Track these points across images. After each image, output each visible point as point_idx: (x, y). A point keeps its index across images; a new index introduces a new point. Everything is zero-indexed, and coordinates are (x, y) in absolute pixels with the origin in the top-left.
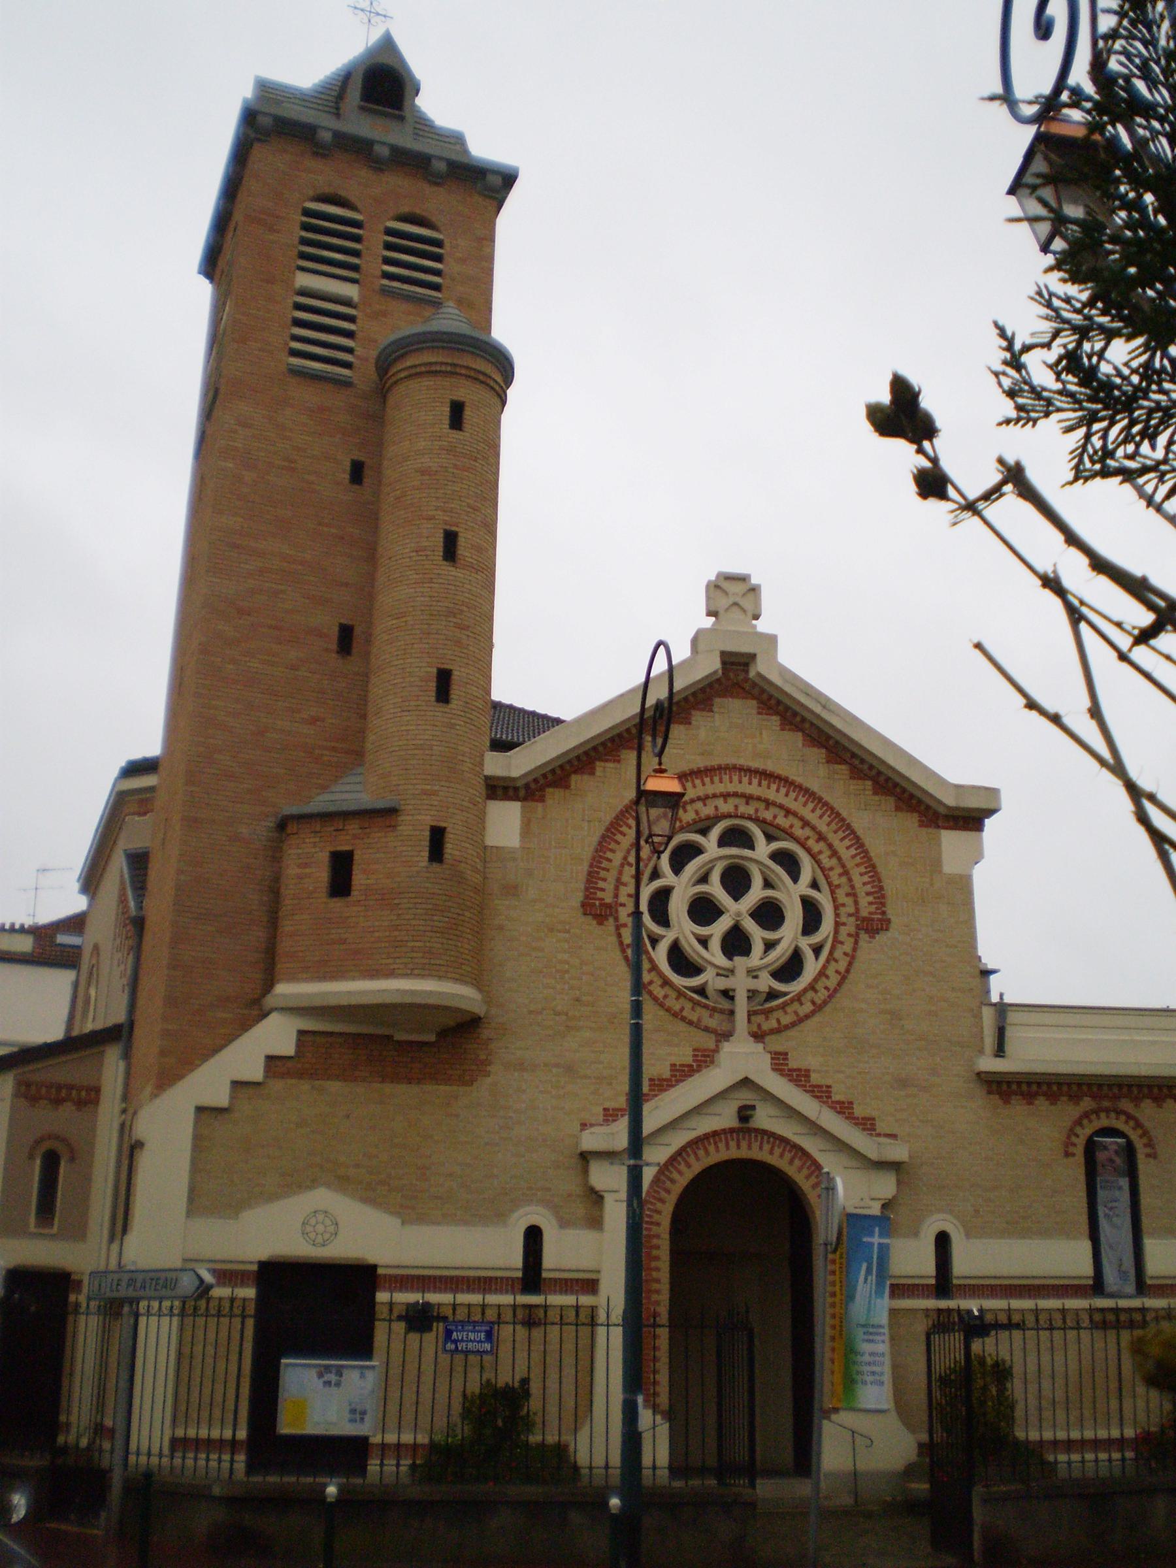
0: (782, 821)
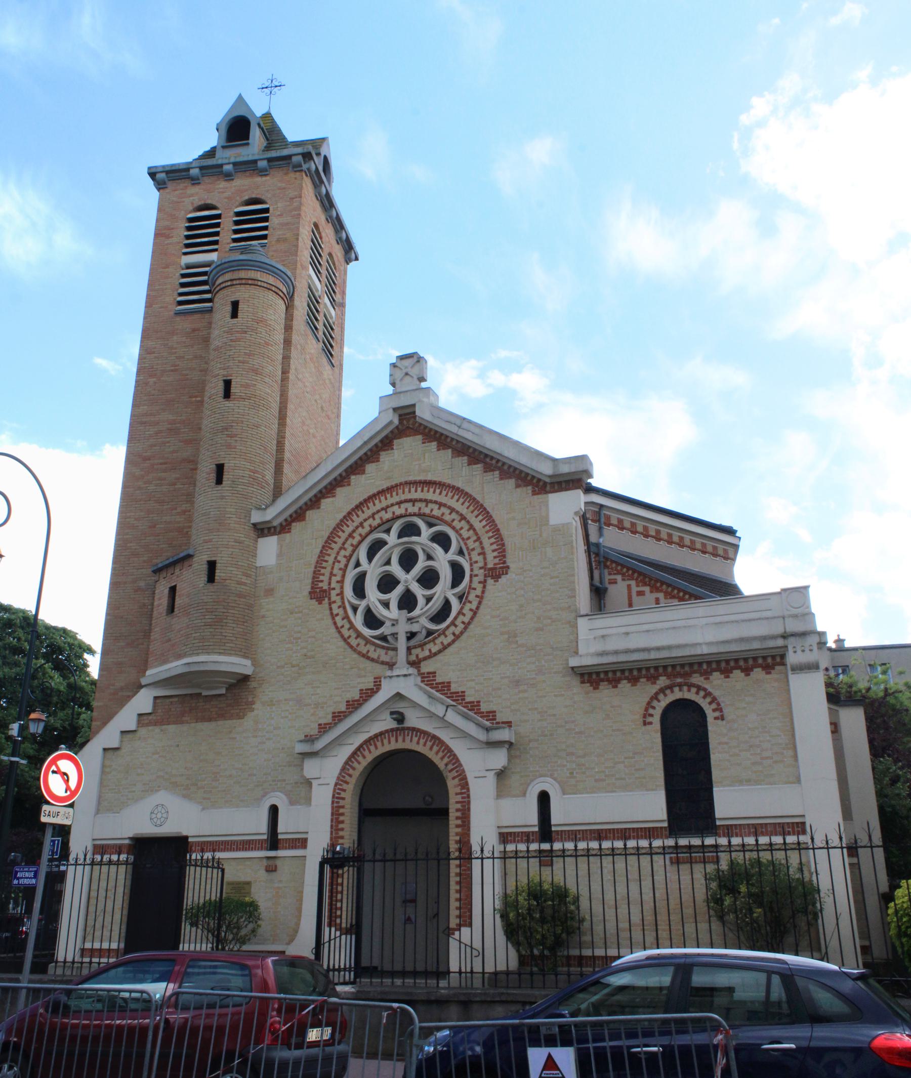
0: (436, 512)
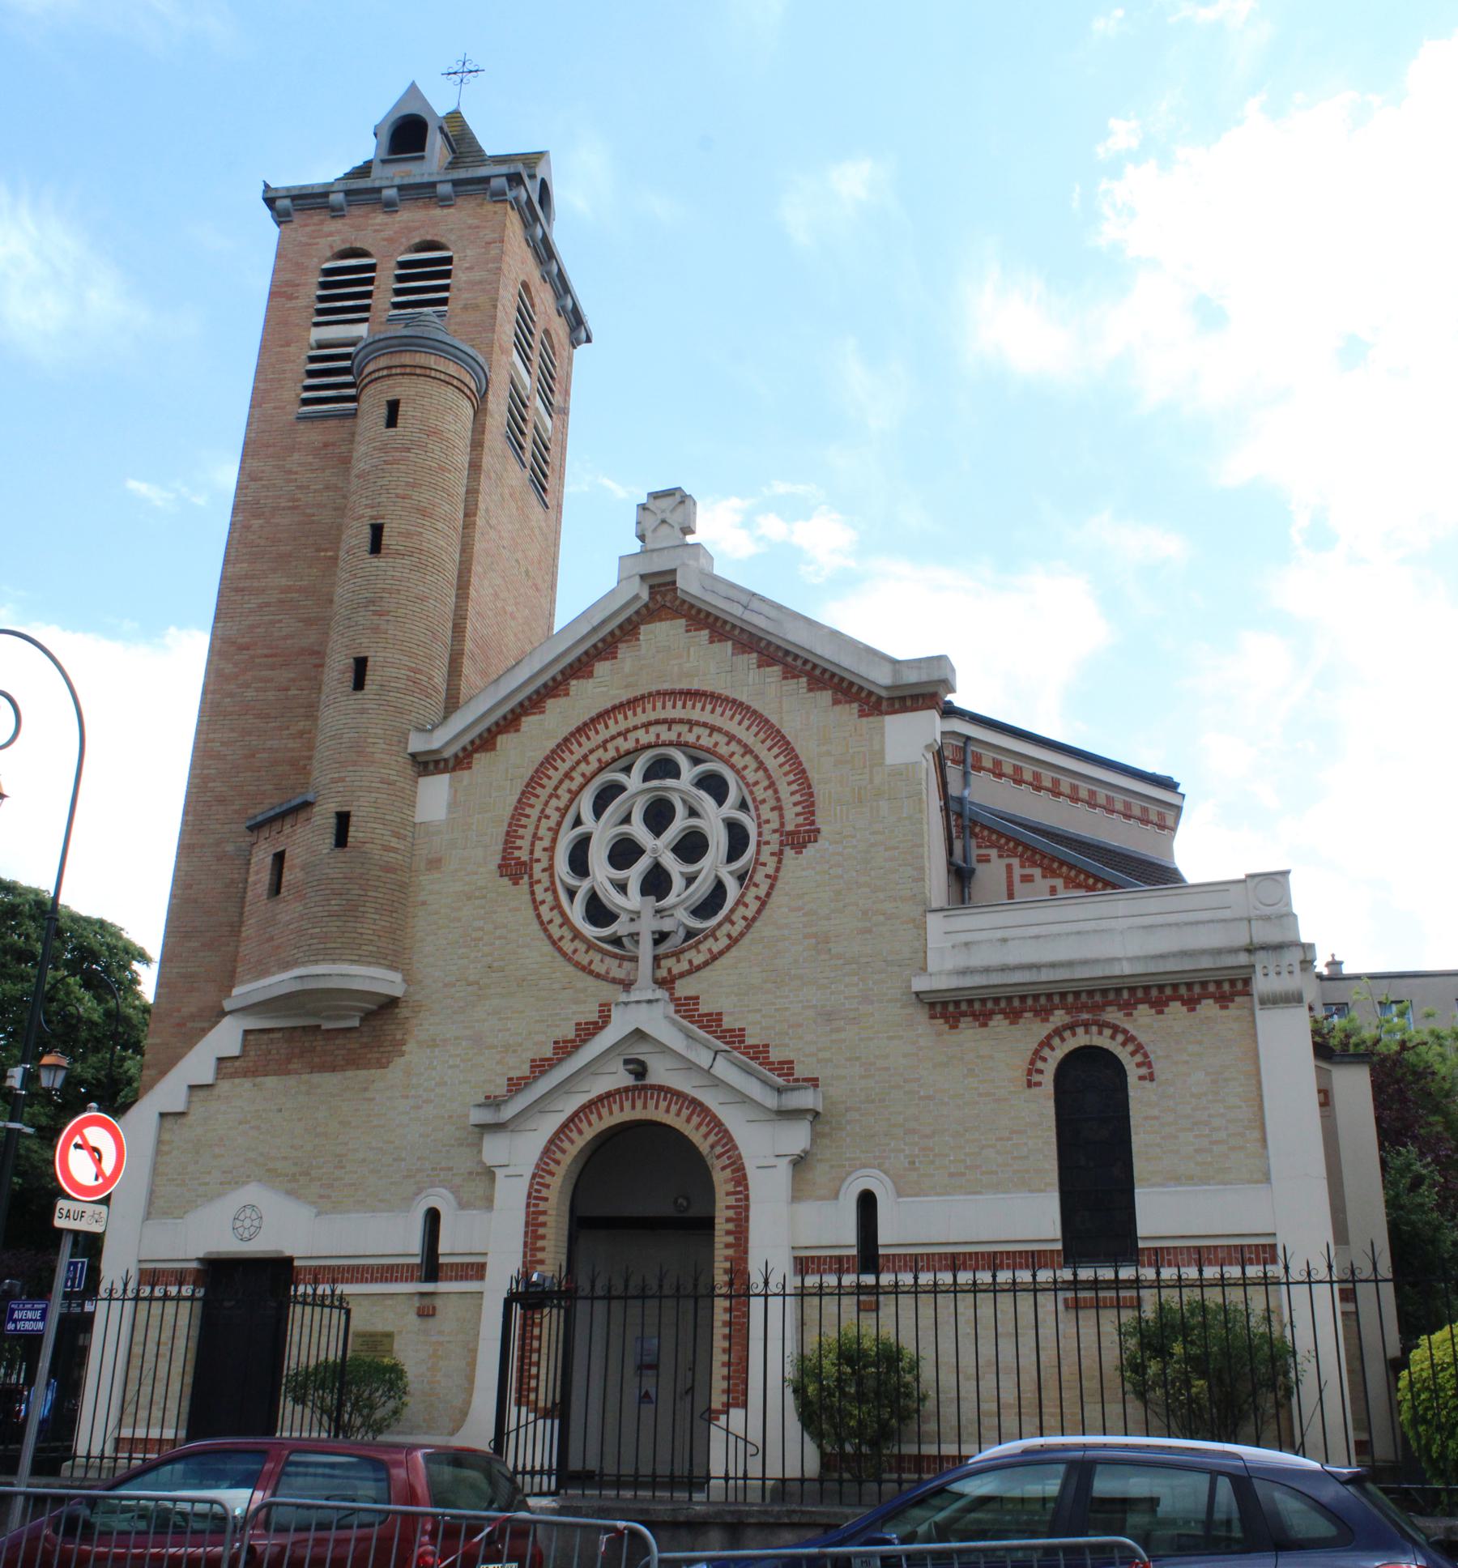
0: (706, 741)
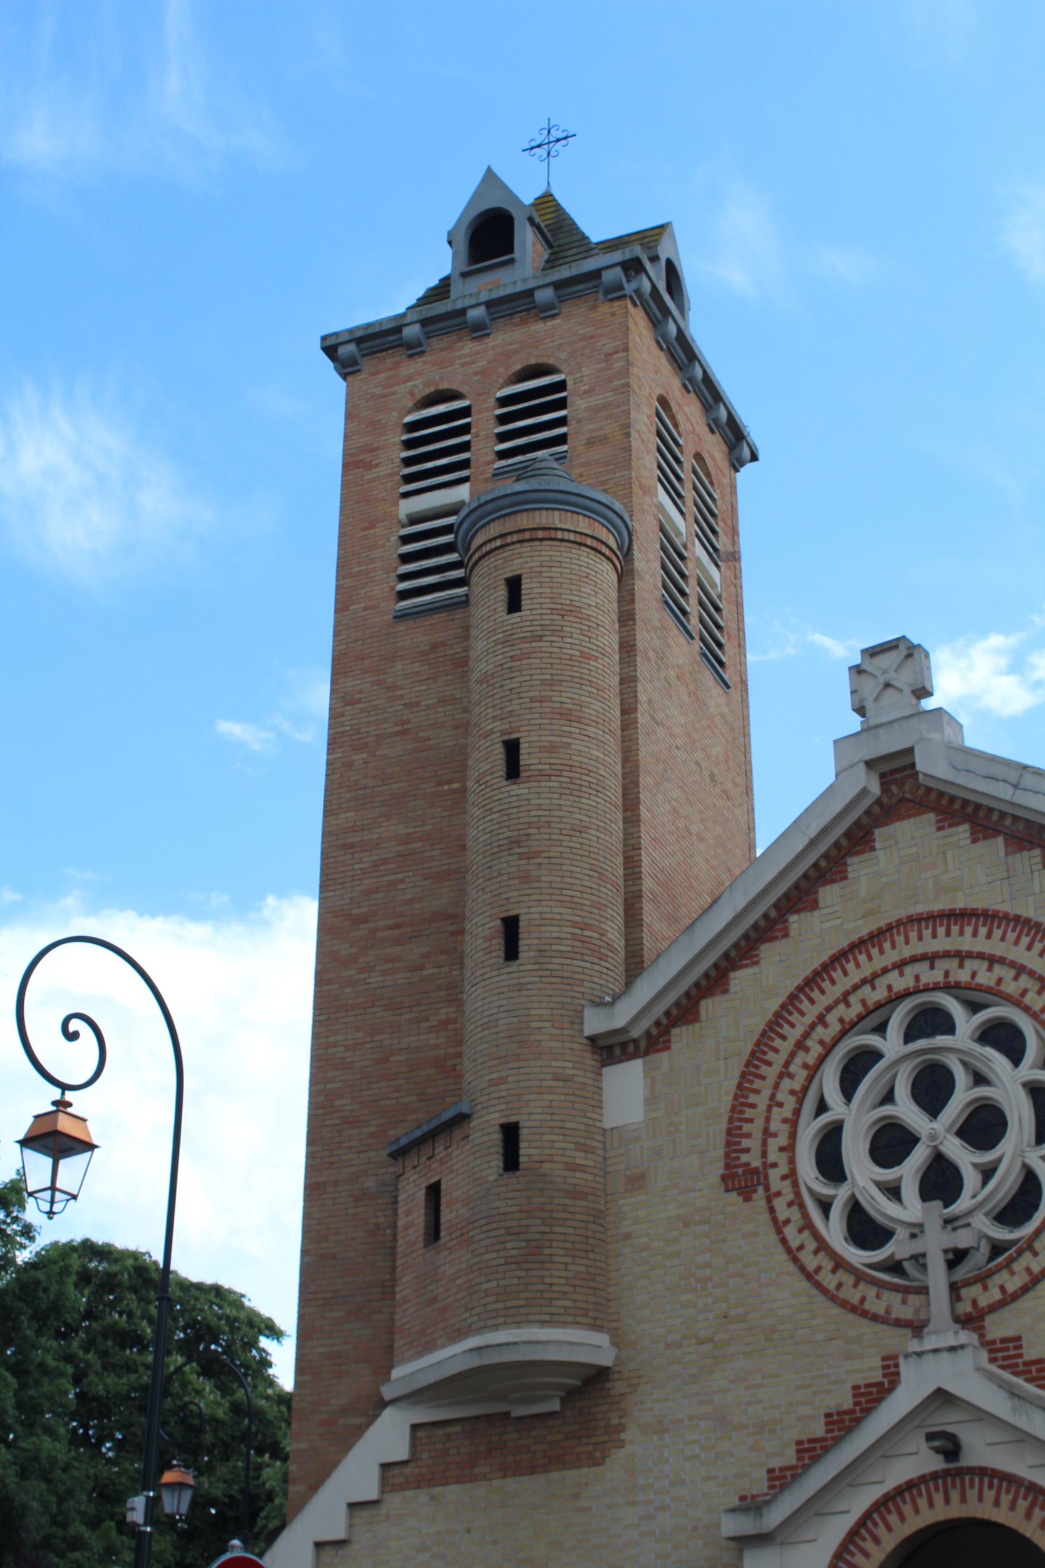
0: (985, 978)
